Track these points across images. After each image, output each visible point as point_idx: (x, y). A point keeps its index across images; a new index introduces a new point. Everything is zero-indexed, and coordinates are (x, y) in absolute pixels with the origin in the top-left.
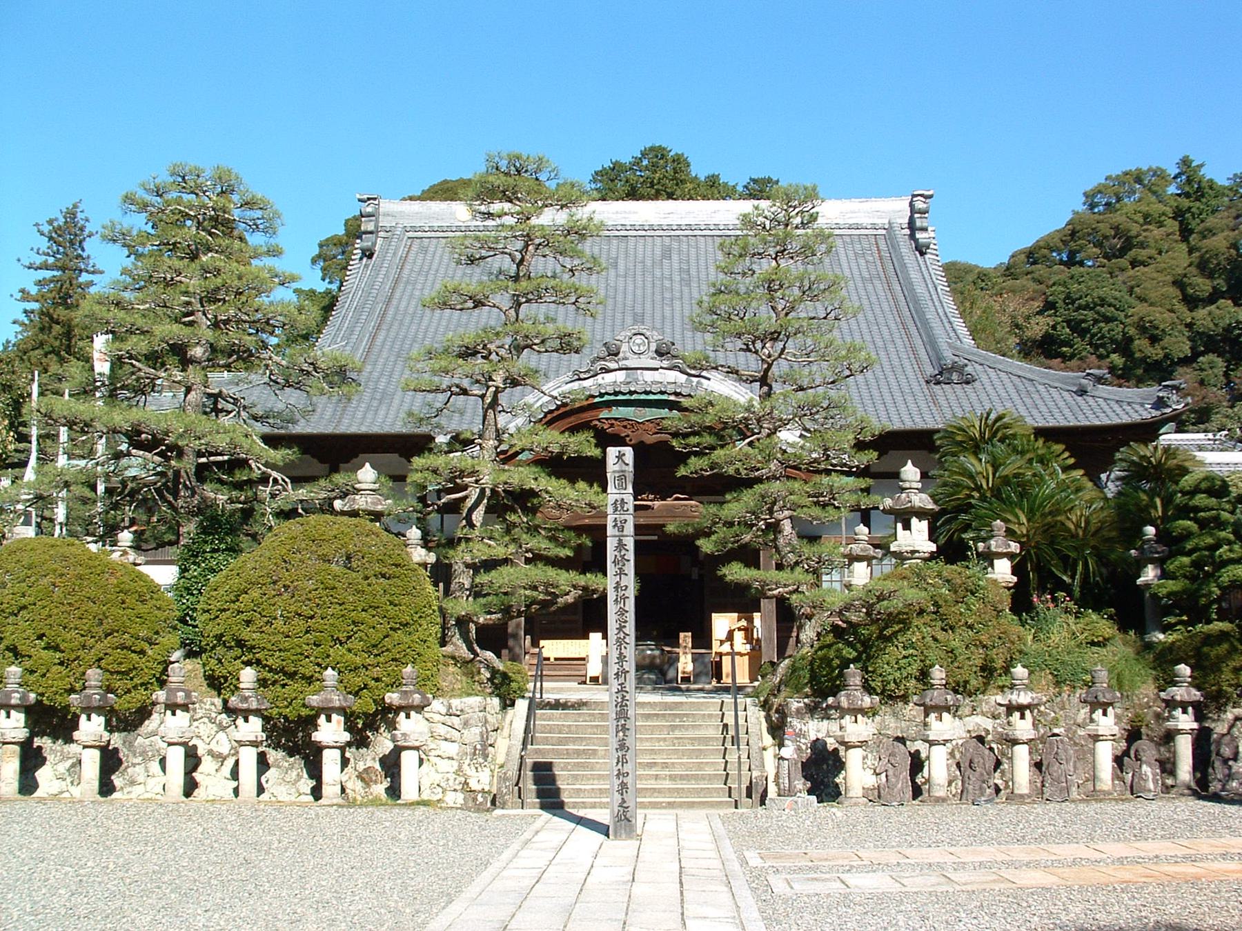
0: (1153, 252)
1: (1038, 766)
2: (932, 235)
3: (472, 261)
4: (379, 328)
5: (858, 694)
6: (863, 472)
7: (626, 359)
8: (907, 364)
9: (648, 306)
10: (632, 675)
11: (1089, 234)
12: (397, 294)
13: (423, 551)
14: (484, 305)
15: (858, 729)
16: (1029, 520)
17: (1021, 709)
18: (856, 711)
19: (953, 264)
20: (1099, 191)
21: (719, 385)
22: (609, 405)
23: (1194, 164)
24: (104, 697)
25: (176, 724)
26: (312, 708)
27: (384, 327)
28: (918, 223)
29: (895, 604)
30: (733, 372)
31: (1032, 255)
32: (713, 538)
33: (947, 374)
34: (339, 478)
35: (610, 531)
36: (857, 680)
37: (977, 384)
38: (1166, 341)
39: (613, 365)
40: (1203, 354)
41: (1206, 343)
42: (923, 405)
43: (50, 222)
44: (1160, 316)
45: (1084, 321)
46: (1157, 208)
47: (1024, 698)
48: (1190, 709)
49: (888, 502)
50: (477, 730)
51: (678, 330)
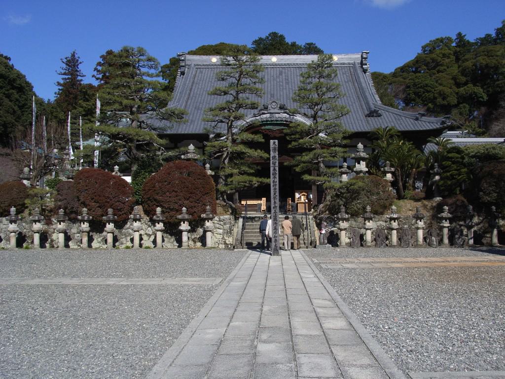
0: (445, 67)
1: (400, 239)
2: (368, 66)
3: (223, 79)
4: (188, 99)
5: (344, 214)
6: (345, 146)
7: (270, 110)
8: (359, 110)
9: (275, 91)
10: (278, 208)
11: (423, 62)
12: (194, 88)
13: (210, 171)
14: (227, 94)
15: (343, 225)
16: (398, 161)
17: (394, 219)
18: (343, 220)
19: (375, 73)
20: (427, 46)
21: (299, 118)
22: (268, 124)
23: (462, 35)
24: (114, 217)
25: (136, 224)
26: (179, 219)
27: (190, 98)
28: (364, 62)
29: (356, 187)
30: (305, 115)
31: (403, 69)
32: (299, 167)
33: (373, 114)
34: (182, 149)
35: (271, 165)
36: (344, 210)
37: (382, 117)
38: (448, 99)
39: (266, 112)
40: (462, 103)
41: (462, 99)
42: (364, 124)
43: (66, 58)
44: (447, 90)
45: (420, 92)
46: (447, 51)
47: (395, 216)
48: (448, 221)
49: (353, 155)
50: (228, 226)
51: (285, 100)
